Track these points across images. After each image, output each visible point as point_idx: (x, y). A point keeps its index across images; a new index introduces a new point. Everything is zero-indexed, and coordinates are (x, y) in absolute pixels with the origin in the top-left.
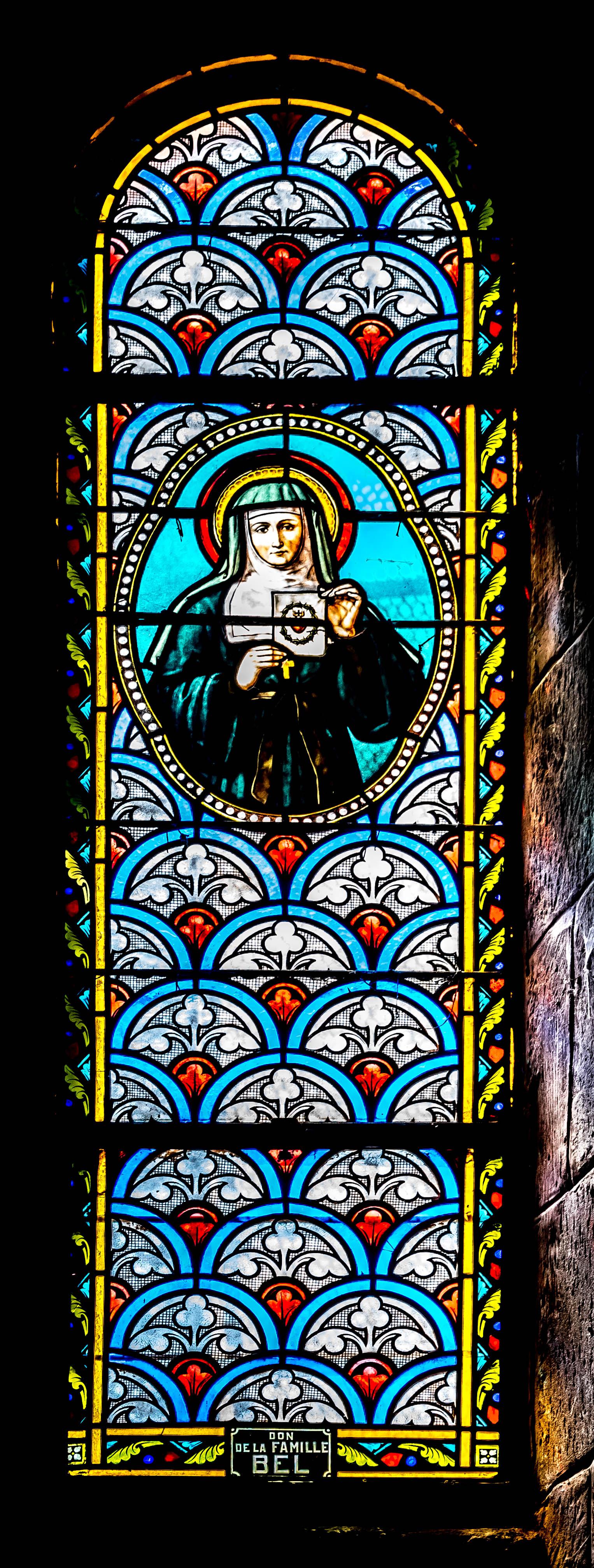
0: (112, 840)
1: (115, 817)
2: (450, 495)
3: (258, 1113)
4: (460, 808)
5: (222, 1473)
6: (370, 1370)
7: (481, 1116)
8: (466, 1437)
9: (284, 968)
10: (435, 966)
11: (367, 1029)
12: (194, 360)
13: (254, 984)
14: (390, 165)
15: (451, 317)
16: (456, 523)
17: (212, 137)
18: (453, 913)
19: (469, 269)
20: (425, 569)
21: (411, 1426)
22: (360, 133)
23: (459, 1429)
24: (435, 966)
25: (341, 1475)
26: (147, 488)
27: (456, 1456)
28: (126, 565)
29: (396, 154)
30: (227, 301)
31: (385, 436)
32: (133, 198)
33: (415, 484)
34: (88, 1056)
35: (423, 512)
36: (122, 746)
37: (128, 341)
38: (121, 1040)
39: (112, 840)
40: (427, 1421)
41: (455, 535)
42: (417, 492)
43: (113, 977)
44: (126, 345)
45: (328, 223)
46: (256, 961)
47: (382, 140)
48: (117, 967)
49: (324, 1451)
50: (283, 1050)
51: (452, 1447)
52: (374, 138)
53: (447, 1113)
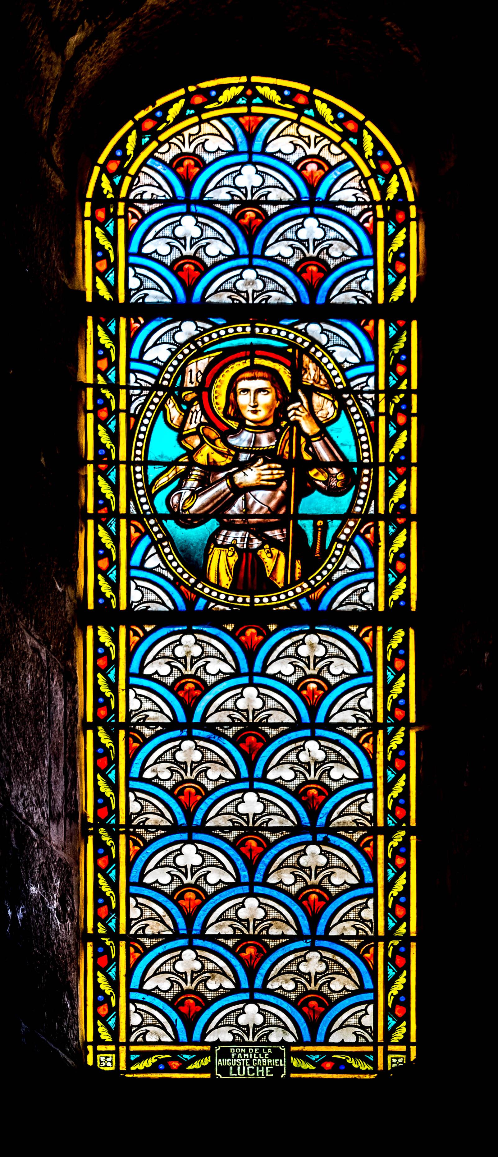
0: (131, 841)
1: (132, 932)
2: (368, 379)
3: (234, 1034)
4: (375, 294)
5: (208, 1076)
6: (314, 896)
7: (390, 510)
8: (380, 1049)
9: (251, 824)
10: (357, 719)
11: (310, 868)
12: (189, 291)
13: (230, 943)
14: (325, 154)
15: (368, 257)
16: (371, 399)
17: (198, 135)
18: (369, 785)
19: (381, 225)
20: (350, 501)
21: (342, 1043)
22: (303, 131)
23: (375, 1044)
24: (357, 719)
25: (293, 1075)
26: (155, 371)
27: (374, 1064)
28: (141, 426)
29: (329, 145)
30: (213, 774)
31: (323, 340)
32: (144, 179)
33: (343, 371)
34: (114, 865)
35: (348, 389)
36: (137, 881)
37: (142, 699)
38: (138, 770)
39: (131, 841)
40: (353, 1039)
41: (371, 406)
42: (345, 377)
43: (132, 830)
44: (141, 701)
45: (281, 822)
46: (231, 820)
47: (318, 135)
48: (135, 823)
49: (281, 1065)
50: (250, 152)
51: (371, 1058)
52: (313, 134)
53: (367, 929)
